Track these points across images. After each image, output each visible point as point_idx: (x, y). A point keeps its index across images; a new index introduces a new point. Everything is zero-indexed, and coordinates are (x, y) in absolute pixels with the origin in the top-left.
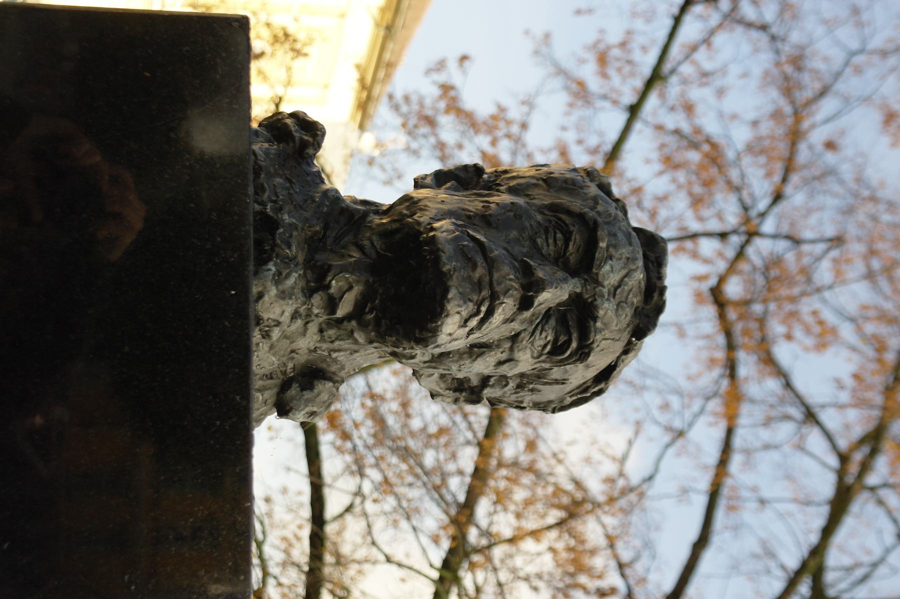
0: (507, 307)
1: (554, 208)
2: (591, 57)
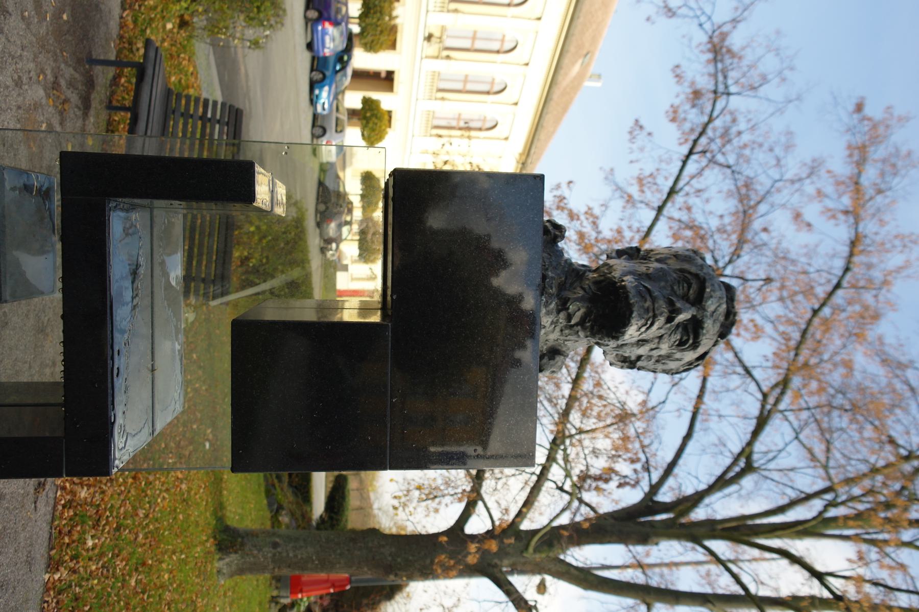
0: (661, 321)
1: (682, 271)
2: (634, 182)
